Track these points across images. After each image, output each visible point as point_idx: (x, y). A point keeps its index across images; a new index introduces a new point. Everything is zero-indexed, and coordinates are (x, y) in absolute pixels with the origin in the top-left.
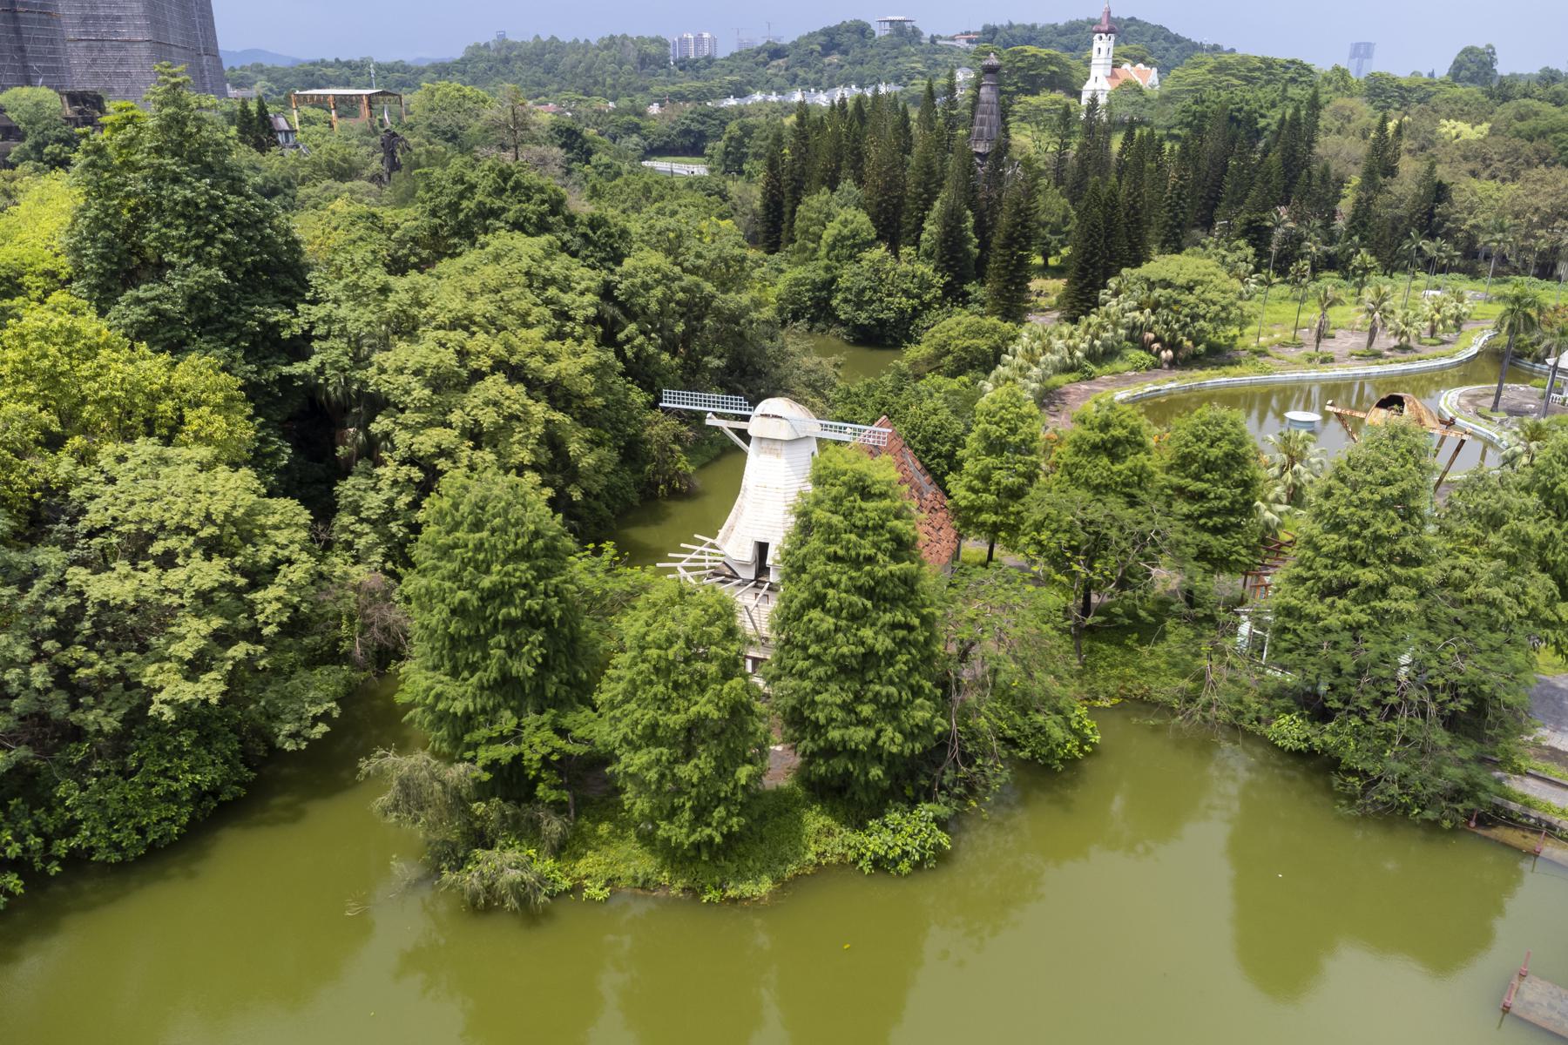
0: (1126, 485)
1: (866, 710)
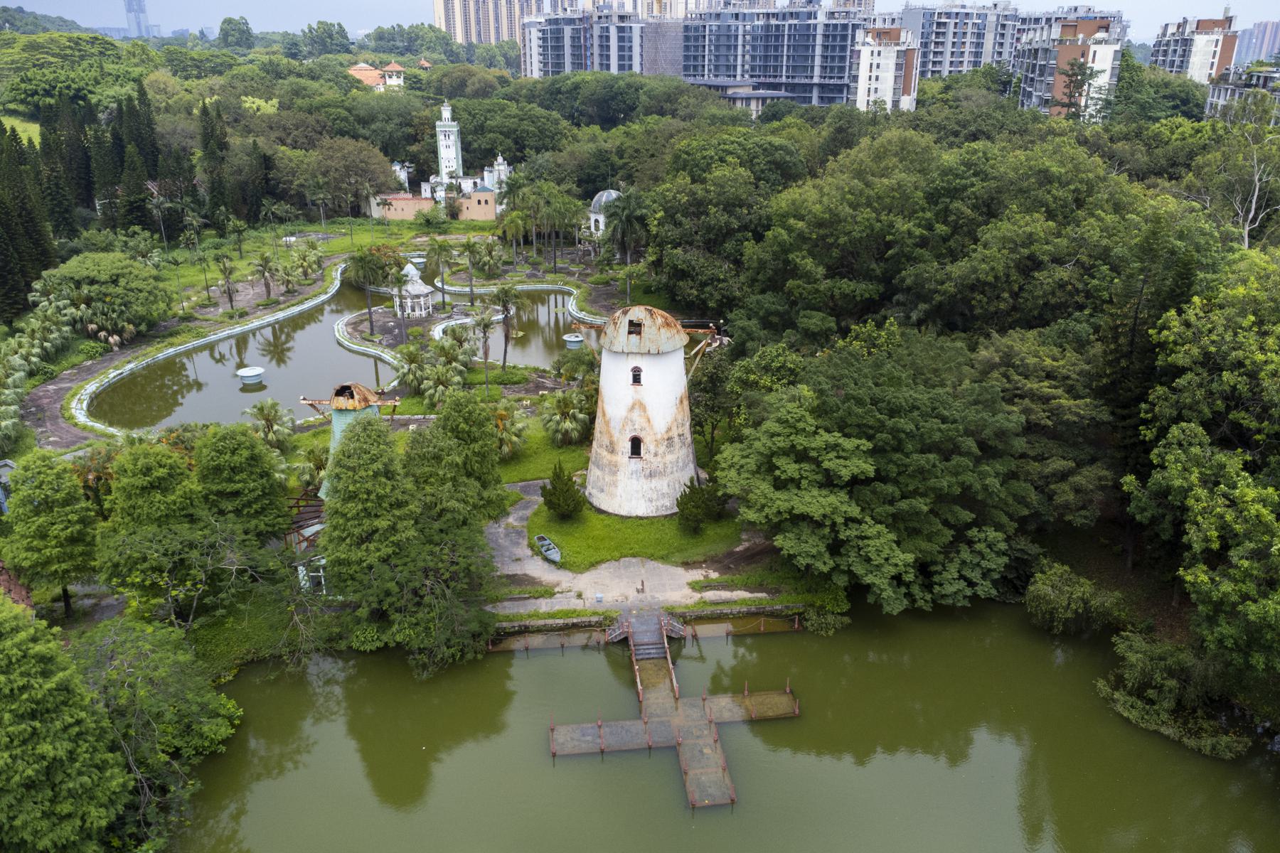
0: (183, 509)
1: (65, 808)
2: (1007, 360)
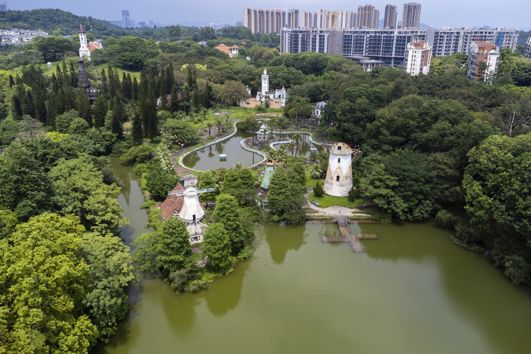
2: (435, 160)
